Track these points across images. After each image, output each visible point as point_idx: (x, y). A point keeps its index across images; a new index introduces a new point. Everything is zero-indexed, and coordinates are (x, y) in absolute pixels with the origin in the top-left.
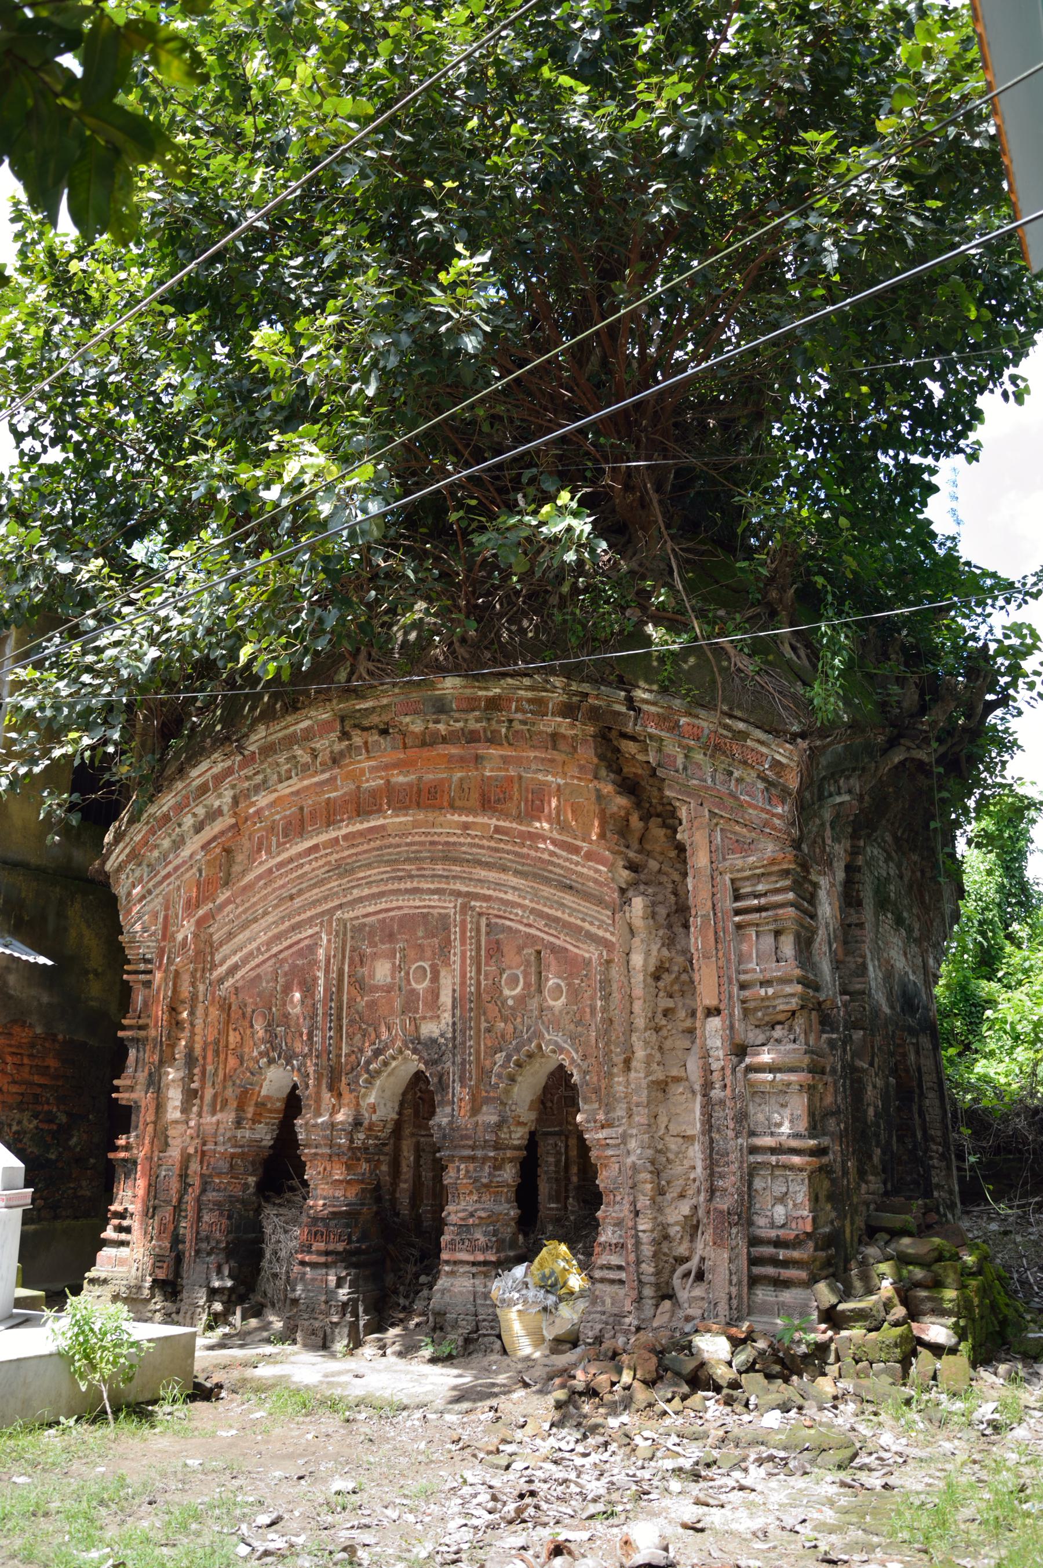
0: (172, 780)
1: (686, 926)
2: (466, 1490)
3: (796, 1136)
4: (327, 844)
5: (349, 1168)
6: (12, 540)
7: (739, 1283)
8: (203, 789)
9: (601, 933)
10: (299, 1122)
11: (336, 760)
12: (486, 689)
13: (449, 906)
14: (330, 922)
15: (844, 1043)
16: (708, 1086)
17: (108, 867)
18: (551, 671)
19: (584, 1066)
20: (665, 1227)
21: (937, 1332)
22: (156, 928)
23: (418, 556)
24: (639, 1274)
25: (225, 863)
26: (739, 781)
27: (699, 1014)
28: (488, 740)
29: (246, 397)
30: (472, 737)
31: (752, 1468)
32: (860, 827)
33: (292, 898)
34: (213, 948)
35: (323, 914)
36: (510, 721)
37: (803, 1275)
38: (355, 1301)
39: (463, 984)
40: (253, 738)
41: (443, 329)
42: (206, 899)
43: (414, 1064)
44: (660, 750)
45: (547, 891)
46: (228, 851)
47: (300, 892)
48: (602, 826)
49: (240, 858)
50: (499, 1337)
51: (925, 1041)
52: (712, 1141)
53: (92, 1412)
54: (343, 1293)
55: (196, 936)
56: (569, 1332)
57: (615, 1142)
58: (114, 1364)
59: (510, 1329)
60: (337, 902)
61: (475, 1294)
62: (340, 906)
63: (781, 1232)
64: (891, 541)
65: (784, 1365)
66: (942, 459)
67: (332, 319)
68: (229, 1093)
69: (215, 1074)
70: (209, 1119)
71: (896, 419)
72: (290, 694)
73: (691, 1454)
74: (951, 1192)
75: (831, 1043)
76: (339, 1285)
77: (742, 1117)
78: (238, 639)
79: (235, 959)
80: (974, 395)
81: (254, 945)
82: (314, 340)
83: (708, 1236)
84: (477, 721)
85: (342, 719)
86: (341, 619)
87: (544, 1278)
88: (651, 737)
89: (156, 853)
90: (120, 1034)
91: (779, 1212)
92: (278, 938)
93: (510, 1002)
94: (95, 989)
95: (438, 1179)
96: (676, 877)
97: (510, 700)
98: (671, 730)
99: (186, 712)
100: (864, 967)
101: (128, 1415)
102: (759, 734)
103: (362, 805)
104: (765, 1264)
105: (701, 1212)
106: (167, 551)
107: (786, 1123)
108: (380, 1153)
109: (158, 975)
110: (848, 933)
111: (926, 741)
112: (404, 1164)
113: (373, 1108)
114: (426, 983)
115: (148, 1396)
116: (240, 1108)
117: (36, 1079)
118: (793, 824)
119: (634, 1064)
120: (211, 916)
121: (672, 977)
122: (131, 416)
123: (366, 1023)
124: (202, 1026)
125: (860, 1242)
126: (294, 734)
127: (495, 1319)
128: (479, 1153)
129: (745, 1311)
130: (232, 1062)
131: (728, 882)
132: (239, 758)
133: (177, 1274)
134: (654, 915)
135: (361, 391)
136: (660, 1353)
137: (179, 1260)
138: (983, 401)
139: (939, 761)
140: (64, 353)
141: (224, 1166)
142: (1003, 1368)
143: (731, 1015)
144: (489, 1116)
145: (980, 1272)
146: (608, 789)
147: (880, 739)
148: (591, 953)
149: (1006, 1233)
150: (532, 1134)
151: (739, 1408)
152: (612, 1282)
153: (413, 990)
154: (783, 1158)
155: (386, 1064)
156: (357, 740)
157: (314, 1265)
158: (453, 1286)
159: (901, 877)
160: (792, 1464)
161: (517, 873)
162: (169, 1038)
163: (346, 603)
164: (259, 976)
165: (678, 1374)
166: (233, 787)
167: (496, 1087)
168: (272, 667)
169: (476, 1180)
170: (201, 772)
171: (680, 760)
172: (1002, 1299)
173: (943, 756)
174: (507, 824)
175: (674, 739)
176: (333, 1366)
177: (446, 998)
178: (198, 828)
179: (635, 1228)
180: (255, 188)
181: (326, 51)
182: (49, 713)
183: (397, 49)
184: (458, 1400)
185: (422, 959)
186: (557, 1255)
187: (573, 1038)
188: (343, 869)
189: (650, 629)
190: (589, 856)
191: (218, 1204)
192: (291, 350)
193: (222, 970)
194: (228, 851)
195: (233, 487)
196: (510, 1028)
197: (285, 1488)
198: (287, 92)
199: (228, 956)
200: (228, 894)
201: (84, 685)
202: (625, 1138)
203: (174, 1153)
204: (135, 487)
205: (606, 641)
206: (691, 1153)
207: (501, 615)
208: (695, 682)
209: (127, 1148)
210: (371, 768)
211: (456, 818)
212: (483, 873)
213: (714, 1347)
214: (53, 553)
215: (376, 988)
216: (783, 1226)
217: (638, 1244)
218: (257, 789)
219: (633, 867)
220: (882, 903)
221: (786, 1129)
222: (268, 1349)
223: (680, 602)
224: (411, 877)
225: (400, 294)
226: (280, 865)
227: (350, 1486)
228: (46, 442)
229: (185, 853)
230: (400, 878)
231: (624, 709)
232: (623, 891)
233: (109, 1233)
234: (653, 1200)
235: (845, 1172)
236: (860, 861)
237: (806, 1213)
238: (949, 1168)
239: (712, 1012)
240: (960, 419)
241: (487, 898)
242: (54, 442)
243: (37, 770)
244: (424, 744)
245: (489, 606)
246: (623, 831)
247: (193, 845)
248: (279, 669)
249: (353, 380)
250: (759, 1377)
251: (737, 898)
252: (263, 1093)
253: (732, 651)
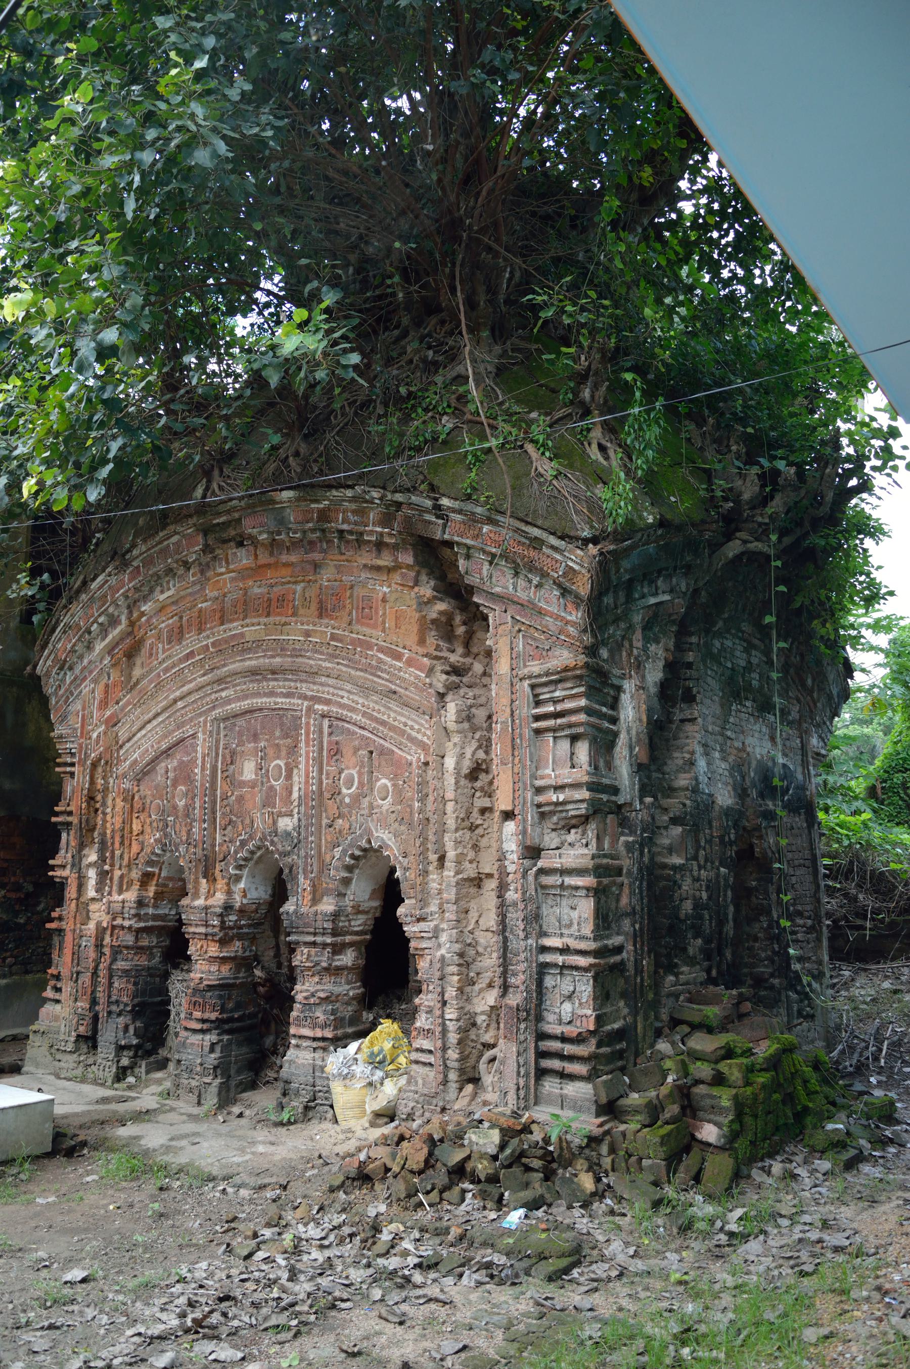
7: (527, 1075)
12: (317, 501)
15: (642, 846)
39: (307, 782)
50: (332, 1106)
56: (385, 1108)
61: (314, 1067)
69: (122, 856)
77: (536, 917)
90: (54, 819)
91: (567, 1007)
93: (347, 800)
102: (553, 540)
110: (660, 734)
118: (585, 631)
119: (447, 864)
128: (319, 939)
129: (532, 1101)
131: (527, 689)
133: (95, 1031)
137: (96, 1019)
143: (525, 820)
149: (896, 992)
153: (272, 787)
157: (195, 1031)
158: (298, 1059)
169: (317, 964)
179: (442, 1016)
185: (278, 758)
190: (410, 663)
215: (243, 784)
216: (570, 1022)
217: (444, 1032)
219: (456, 671)
232: (441, 696)
233: (49, 993)
234: (460, 990)
235: (639, 970)
237: (589, 1012)
239: (508, 815)
251: (538, 703)
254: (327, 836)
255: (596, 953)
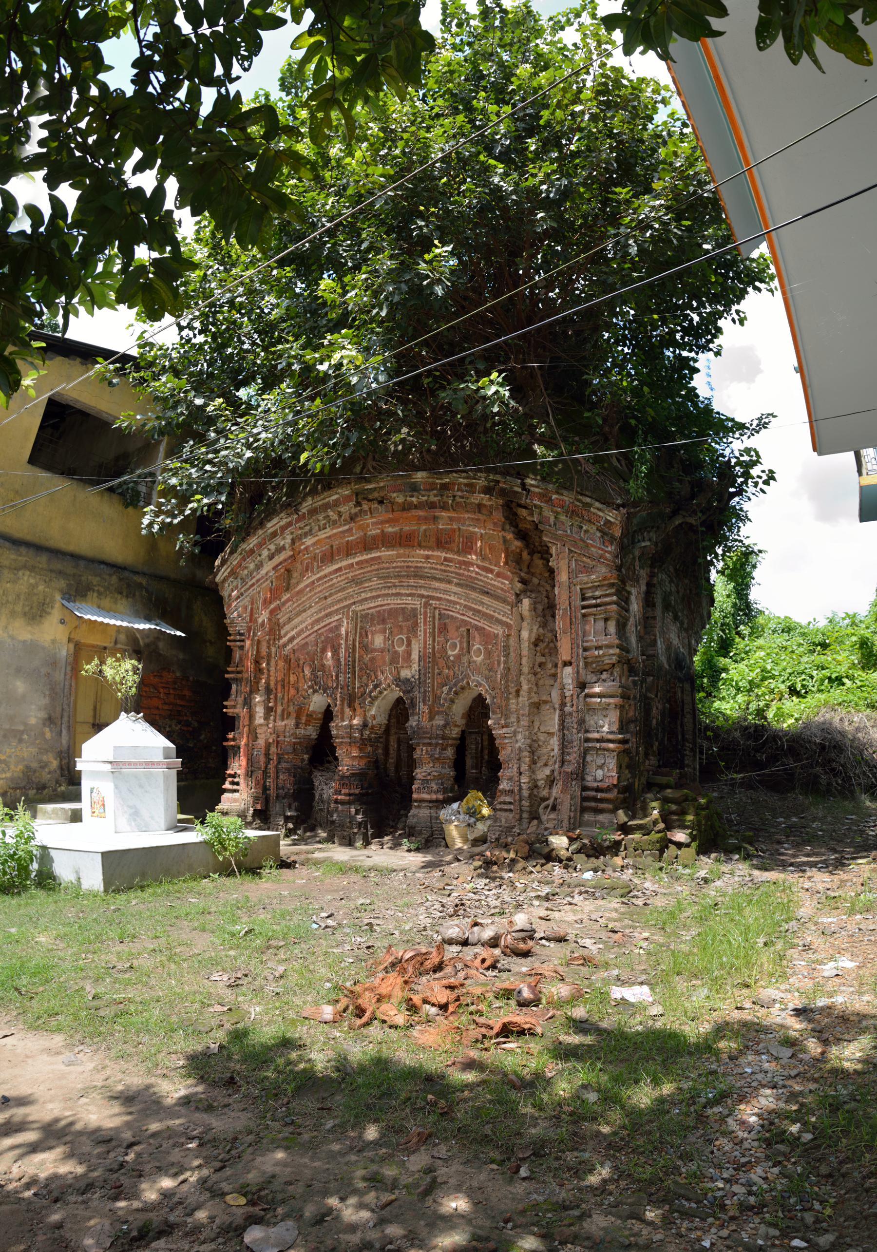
0: (256, 529)
1: (554, 616)
2: (428, 904)
3: (611, 733)
4: (346, 567)
5: (360, 749)
6: (169, 385)
7: (575, 810)
8: (274, 534)
9: (504, 619)
10: (332, 724)
11: (352, 518)
13: (417, 603)
14: (348, 612)
16: (563, 705)
17: (217, 579)
18: (480, 470)
19: (493, 694)
20: (536, 781)
21: (680, 836)
22: (246, 616)
23: (404, 402)
24: (521, 806)
25: (286, 577)
26: (586, 531)
27: (560, 665)
28: (441, 507)
29: (314, 313)
30: (432, 506)
31: (576, 896)
32: (656, 561)
33: (326, 598)
34: (280, 627)
35: (344, 607)
36: (454, 496)
37: (611, 806)
38: (365, 823)
39: (425, 647)
40: (305, 505)
41: (425, 283)
42: (275, 599)
43: (397, 693)
44: (540, 514)
45: (474, 595)
46: (288, 571)
47: (331, 595)
48: (506, 557)
49: (295, 575)
50: (444, 839)
51: (687, 686)
52: (564, 735)
53: (226, 870)
54: (359, 818)
55: (269, 620)
56: (482, 836)
57: (510, 735)
58: (236, 847)
59: (450, 834)
60: (352, 601)
61: (431, 817)
62: (354, 603)
63: (600, 784)
64: (673, 399)
65: (596, 851)
66: (700, 355)
67: (364, 276)
68: (291, 709)
69: (283, 698)
70: (280, 724)
71: (673, 332)
72: (327, 480)
73: (545, 890)
74: (695, 769)
75: (635, 683)
76: (357, 813)
77: (581, 722)
78: (299, 449)
79: (293, 633)
80: (716, 320)
81: (304, 625)
82: (353, 288)
83: (560, 786)
84: (435, 496)
85: (357, 494)
86: (360, 439)
87: (469, 809)
88: (535, 506)
89: (246, 572)
90: (226, 676)
92: (318, 621)
94: (210, 651)
95: (410, 756)
96: (549, 588)
97: (454, 484)
98: (547, 502)
99: (265, 489)
100: (655, 641)
101: (247, 872)
102: (597, 504)
103: (367, 544)
104: (589, 802)
105: (556, 773)
106: (260, 395)
107: (606, 725)
108: (378, 742)
109: (248, 643)
110: (647, 621)
111: (695, 512)
112: (391, 749)
113: (374, 717)
114: (404, 647)
115: (257, 865)
116: (298, 717)
117: (178, 702)
119: (521, 693)
120: (278, 608)
121: (545, 645)
122: (246, 319)
123: (370, 670)
124: (274, 671)
125: (643, 791)
126: (329, 503)
127: (442, 830)
128: (434, 741)
130: (292, 692)
132: (296, 516)
134: (535, 609)
135: (378, 313)
136: (531, 844)
138: (721, 323)
139: (702, 524)
140: (213, 285)
141: (289, 749)
142: (713, 855)
143: (578, 666)
144: (439, 721)
145: (707, 808)
146: (510, 536)
147: (668, 510)
148: (499, 630)
150: (463, 732)
151: (571, 870)
152: (506, 810)
153: (396, 652)
154: (604, 745)
155: (381, 693)
156: (365, 507)
157: (342, 803)
158: (419, 814)
159: (678, 592)
160: (597, 895)
161: (457, 585)
162: (255, 677)
163: (363, 429)
164: (307, 643)
165: (540, 854)
166: (292, 533)
167: (443, 705)
168: (319, 465)
170: (273, 525)
171: (552, 519)
172: (717, 824)
173: (704, 521)
174: (451, 556)
175: (548, 507)
176: (355, 853)
177: (415, 656)
178: (271, 557)
180: (328, 207)
181: (371, 145)
182: (184, 487)
183: (407, 145)
184: (423, 867)
186: (475, 798)
187: (487, 678)
188: (356, 581)
189: (536, 447)
190: (498, 575)
191: (288, 770)
192: (340, 291)
193: (285, 639)
194: (288, 571)
195: (302, 363)
196: (452, 673)
197: (334, 902)
198: (350, 164)
199: (288, 632)
200: (288, 595)
201: (206, 471)
202: (515, 733)
203: (261, 742)
204: (244, 358)
205: (510, 454)
206: (552, 742)
207: (451, 437)
208: (563, 476)
209: (234, 739)
210: (373, 524)
211: (422, 552)
212: (437, 584)
213: (559, 842)
214: (193, 393)
215: (375, 650)
217: (520, 789)
218: (306, 535)
219: (523, 581)
220: (667, 607)
221: (606, 729)
222: (320, 846)
223: (553, 432)
224: (395, 586)
225: (402, 263)
226: (319, 579)
227: (368, 901)
228: (196, 332)
229: (263, 572)
230: (389, 587)
231: (520, 490)
232: (517, 595)
233: (227, 785)
234: (529, 766)
236: (655, 580)
238: (695, 756)
239: (567, 664)
240: (710, 333)
241: (439, 599)
242: (200, 333)
243: (176, 521)
244: (404, 509)
245: (444, 431)
246: (518, 561)
247: (268, 567)
248: (323, 467)
249: (373, 307)
250: (583, 856)
251: (583, 599)
252: (311, 709)
253: (583, 461)
254: (438, 680)
255: (620, 742)
